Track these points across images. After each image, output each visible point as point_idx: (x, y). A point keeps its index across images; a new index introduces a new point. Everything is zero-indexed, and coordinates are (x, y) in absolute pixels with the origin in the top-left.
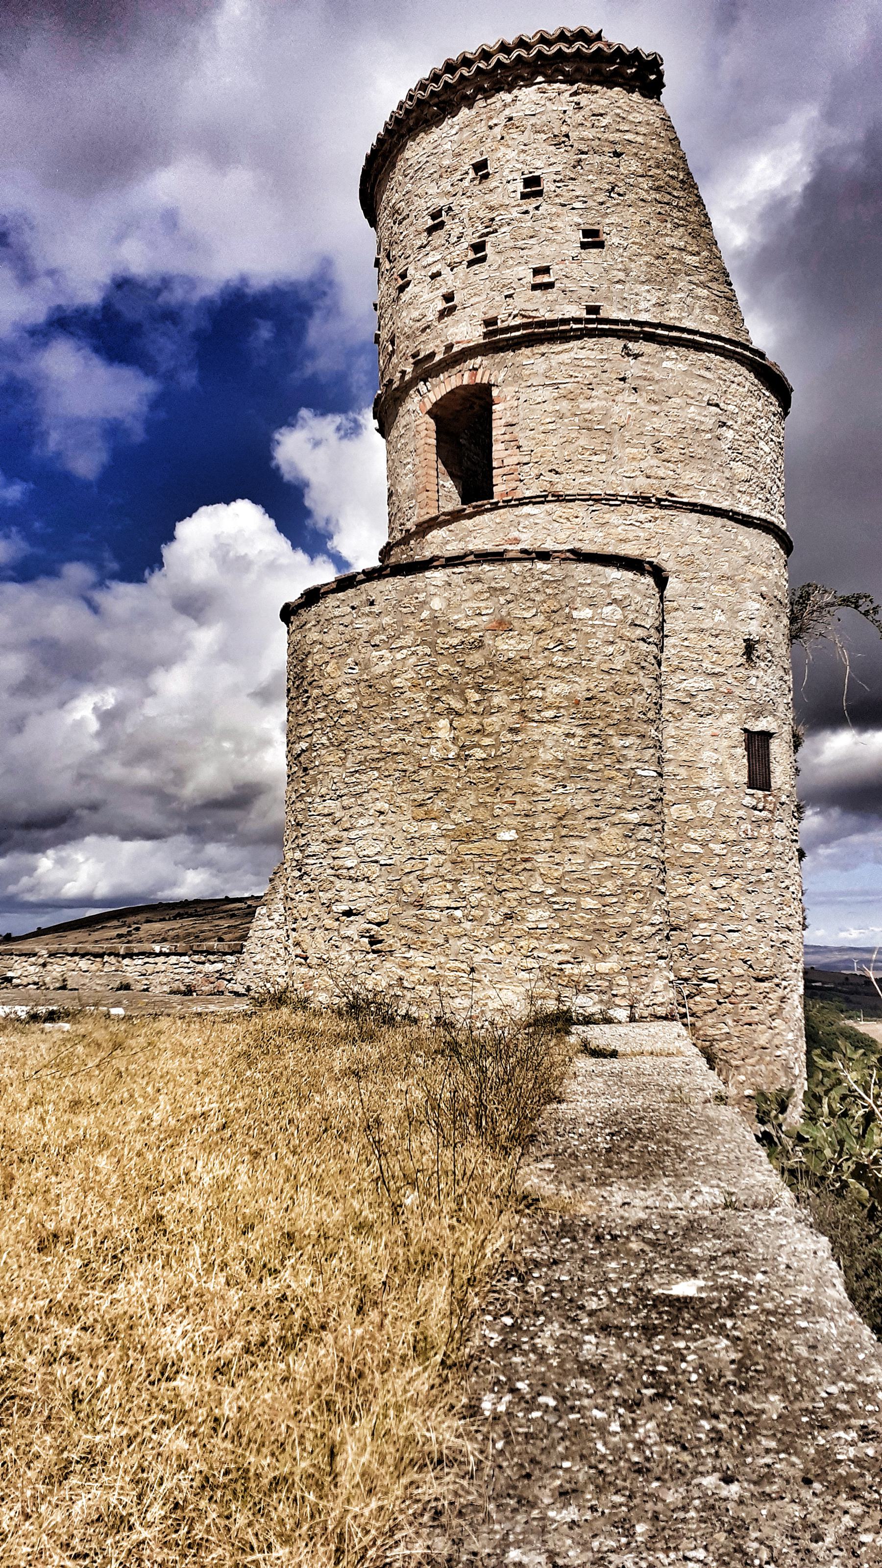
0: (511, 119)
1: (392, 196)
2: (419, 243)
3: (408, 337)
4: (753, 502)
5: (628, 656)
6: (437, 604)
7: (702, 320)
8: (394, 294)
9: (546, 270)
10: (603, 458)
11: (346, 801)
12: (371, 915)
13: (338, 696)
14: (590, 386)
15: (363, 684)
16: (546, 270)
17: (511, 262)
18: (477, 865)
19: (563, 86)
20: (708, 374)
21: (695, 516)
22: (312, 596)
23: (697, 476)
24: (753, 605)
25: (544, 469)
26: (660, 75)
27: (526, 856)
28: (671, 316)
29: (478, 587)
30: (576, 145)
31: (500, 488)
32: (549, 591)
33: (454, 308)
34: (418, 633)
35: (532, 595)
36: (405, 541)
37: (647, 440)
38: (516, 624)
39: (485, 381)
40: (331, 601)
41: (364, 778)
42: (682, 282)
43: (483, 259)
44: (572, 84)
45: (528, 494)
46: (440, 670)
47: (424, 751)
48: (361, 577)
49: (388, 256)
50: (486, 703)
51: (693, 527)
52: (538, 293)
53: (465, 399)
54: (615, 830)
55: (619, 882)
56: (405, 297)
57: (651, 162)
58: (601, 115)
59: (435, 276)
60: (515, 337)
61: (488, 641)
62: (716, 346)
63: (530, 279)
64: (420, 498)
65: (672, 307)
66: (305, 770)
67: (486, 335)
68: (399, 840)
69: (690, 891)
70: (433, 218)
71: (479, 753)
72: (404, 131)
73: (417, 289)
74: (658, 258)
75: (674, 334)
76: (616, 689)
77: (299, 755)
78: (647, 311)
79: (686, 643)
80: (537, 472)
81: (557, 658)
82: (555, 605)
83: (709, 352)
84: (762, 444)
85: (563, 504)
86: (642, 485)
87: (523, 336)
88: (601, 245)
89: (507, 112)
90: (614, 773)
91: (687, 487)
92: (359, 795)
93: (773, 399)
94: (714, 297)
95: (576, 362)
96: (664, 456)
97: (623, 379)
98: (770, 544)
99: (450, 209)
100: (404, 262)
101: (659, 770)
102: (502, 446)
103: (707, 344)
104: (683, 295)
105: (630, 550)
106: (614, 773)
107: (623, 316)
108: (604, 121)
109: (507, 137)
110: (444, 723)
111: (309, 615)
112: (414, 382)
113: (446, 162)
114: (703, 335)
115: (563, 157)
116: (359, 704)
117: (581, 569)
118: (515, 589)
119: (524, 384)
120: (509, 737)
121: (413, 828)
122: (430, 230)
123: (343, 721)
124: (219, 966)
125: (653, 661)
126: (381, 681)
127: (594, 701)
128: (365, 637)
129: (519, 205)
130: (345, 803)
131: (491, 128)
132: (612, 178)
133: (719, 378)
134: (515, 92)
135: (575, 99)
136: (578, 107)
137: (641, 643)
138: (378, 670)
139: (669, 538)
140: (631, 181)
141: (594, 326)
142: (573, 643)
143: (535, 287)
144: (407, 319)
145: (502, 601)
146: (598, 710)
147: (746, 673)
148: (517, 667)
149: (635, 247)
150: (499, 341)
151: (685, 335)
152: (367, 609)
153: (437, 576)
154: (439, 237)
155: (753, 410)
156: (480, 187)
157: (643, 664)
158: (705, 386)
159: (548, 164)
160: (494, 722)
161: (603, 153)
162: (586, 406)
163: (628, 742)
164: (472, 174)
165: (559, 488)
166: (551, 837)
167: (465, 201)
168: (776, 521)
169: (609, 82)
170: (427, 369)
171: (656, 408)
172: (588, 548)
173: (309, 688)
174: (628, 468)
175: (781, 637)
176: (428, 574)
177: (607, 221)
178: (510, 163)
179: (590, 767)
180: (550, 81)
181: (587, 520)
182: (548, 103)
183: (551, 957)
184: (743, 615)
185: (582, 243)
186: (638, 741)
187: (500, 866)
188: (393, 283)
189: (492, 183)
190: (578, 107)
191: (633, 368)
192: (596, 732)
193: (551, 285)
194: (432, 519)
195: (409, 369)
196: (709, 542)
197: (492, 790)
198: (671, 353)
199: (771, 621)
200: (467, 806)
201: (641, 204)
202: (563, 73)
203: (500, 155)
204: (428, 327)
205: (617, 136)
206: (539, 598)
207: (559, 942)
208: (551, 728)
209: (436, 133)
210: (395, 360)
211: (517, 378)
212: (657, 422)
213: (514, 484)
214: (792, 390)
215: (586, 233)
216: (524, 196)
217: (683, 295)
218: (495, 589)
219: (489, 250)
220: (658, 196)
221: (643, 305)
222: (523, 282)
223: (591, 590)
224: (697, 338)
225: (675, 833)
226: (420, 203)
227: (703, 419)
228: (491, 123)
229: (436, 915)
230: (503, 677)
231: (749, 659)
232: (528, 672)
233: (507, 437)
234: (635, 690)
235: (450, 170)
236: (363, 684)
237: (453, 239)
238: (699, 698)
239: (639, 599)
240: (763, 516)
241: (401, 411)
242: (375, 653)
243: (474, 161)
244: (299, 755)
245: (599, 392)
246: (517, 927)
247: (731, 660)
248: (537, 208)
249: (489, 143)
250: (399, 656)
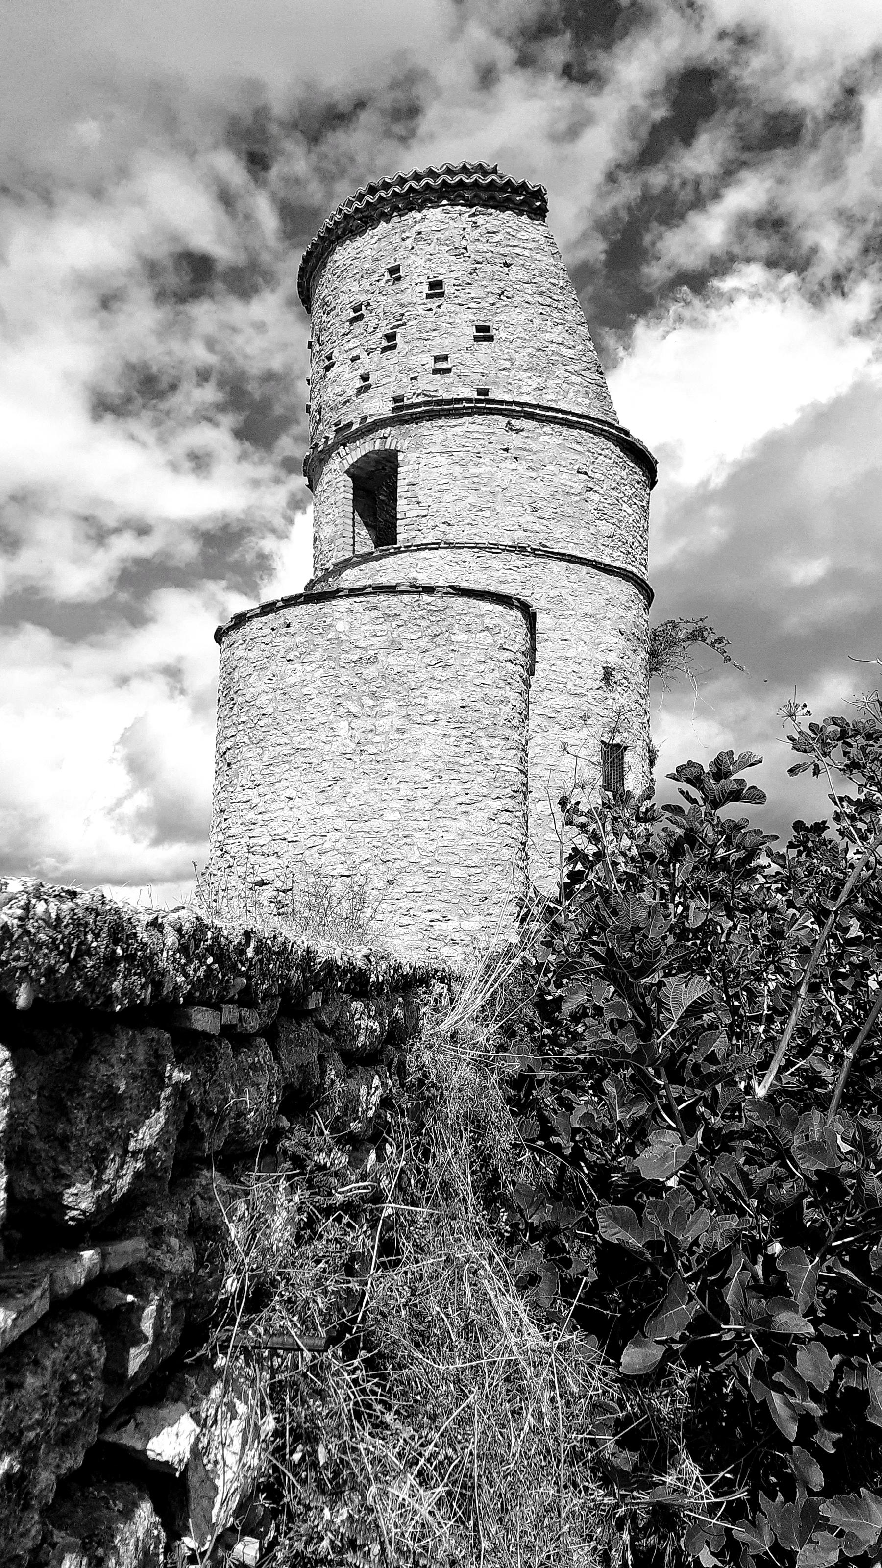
0: (420, 233)
1: (322, 291)
2: (343, 331)
4: (615, 555)
5: (496, 674)
6: (341, 626)
7: (574, 403)
8: (322, 372)
9: (445, 358)
10: (487, 513)
13: (258, 702)
14: (478, 455)
15: (279, 692)
16: (445, 358)
17: (416, 350)
18: (367, 841)
19: (464, 209)
20: (578, 448)
21: (564, 564)
22: (241, 620)
23: (567, 531)
24: (612, 639)
25: (439, 521)
26: (544, 201)
27: (407, 833)
28: (547, 399)
29: (375, 613)
30: (473, 256)
31: (402, 537)
32: (432, 619)
33: (370, 386)
34: (325, 650)
35: (419, 622)
36: (324, 578)
37: (526, 501)
38: (405, 644)
39: (393, 448)
40: (256, 623)
41: (276, 770)
42: (560, 371)
43: (394, 347)
44: (471, 207)
45: (425, 541)
46: (342, 680)
47: (327, 747)
48: (281, 604)
49: (318, 340)
50: (378, 708)
51: (562, 573)
52: (438, 376)
53: (377, 462)
54: (481, 814)
55: (483, 857)
56: (330, 375)
57: (536, 272)
58: (494, 233)
59: (354, 359)
60: (416, 413)
61: (381, 657)
62: (586, 425)
64: (337, 543)
65: (550, 391)
66: (229, 765)
67: (394, 410)
68: (304, 822)
69: (550, 873)
70: (355, 311)
72: (333, 238)
73: (340, 369)
74: (539, 350)
75: (550, 413)
76: (486, 700)
77: (225, 753)
78: (528, 394)
79: (553, 668)
80: (433, 524)
82: (436, 630)
83: (580, 429)
84: (625, 507)
85: (454, 551)
86: (519, 537)
87: (426, 411)
88: (491, 338)
89: (417, 227)
90: (481, 768)
91: (557, 541)
93: (638, 470)
94: (586, 384)
95: (468, 435)
96: (539, 514)
97: (507, 450)
98: (628, 589)
99: (368, 304)
100: (330, 346)
101: (521, 768)
102: (404, 502)
103: (578, 422)
104: (560, 381)
105: (507, 590)
106: (481, 768)
107: (507, 398)
108: (497, 238)
109: (416, 248)
110: (344, 724)
111: (236, 636)
112: (335, 446)
113: (367, 266)
114: (574, 414)
115: (463, 266)
117: (460, 602)
118: (404, 616)
119: (425, 451)
120: (397, 736)
122: (352, 321)
123: (261, 723)
125: (519, 679)
126: (293, 689)
127: (467, 709)
128: (282, 653)
129: (424, 304)
130: (260, 791)
131: (403, 239)
132: (502, 284)
133: (589, 451)
134: (424, 212)
135: (473, 219)
136: (475, 225)
137: (509, 664)
138: (292, 680)
139: (543, 583)
140: (518, 287)
141: (483, 405)
142: (451, 661)
143: (436, 372)
144: (331, 394)
146: (470, 716)
147: (605, 695)
148: (404, 679)
149: (520, 341)
150: (405, 414)
151: (560, 415)
153: (343, 604)
154: (359, 327)
155: (618, 478)
156: (394, 287)
157: (510, 680)
158: (576, 457)
159: (450, 270)
160: (384, 724)
161: (495, 264)
162: (474, 470)
163: (495, 742)
164: (387, 276)
165: (450, 538)
166: (427, 818)
167: (381, 298)
168: (635, 571)
169: (501, 206)
170: (346, 435)
171: (534, 474)
172: (465, 585)
173: (235, 696)
174: (510, 522)
175: (638, 668)
176: (334, 602)
177: (497, 319)
178: (418, 268)
179: (462, 762)
180: (453, 204)
181: (473, 564)
182: (451, 222)
183: (424, 916)
184: (603, 647)
185: (475, 337)
186: (503, 743)
188: (321, 363)
189: (403, 284)
190: (475, 225)
191: (515, 441)
192: (468, 734)
193: (448, 370)
194: (346, 560)
195: (332, 436)
196: (575, 585)
197: (381, 780)
198: (547, 429)
199: (628, 653)
200: (360, 792)
201: (527, 305)
202: (464, 198)
203: (410, 262)
204: (348, 401)
205: (507, 250)
206: (424, 623)
208: (432, 730)
209: (359, 241)
210: (321, 427)
211: (418, 446)
212: (534, 485)
213: (414, 533)
214: (657, 462)
215: (479, 329)
216: (429, 296)
217: (560, 381)
218: (389, 616)
219: (399, 339)
220: (541, 300)
222: (426, 367)
223: (467, 619)
224: (570, 417)
225: (539, 825)
226: (345, 299)
227: (573, 484)
228: (404, 236)
230: (392, 686)
231: (607, 684)
232: (413, 683)
233: (409, 494)
234: (502, 702)
235: (369, 273)
236: (279, 692)
237: (370, 330)
238: (563, 714)
239: (507, 628)
240: (623, 566)
241: (325, 470)
242: (289, 667)
243: (389, 266)
244: (225, 753)
245: (486, 459)
246: (397, 891)
247: (591, 684)
248: (439, 306)
249: (401, 252)
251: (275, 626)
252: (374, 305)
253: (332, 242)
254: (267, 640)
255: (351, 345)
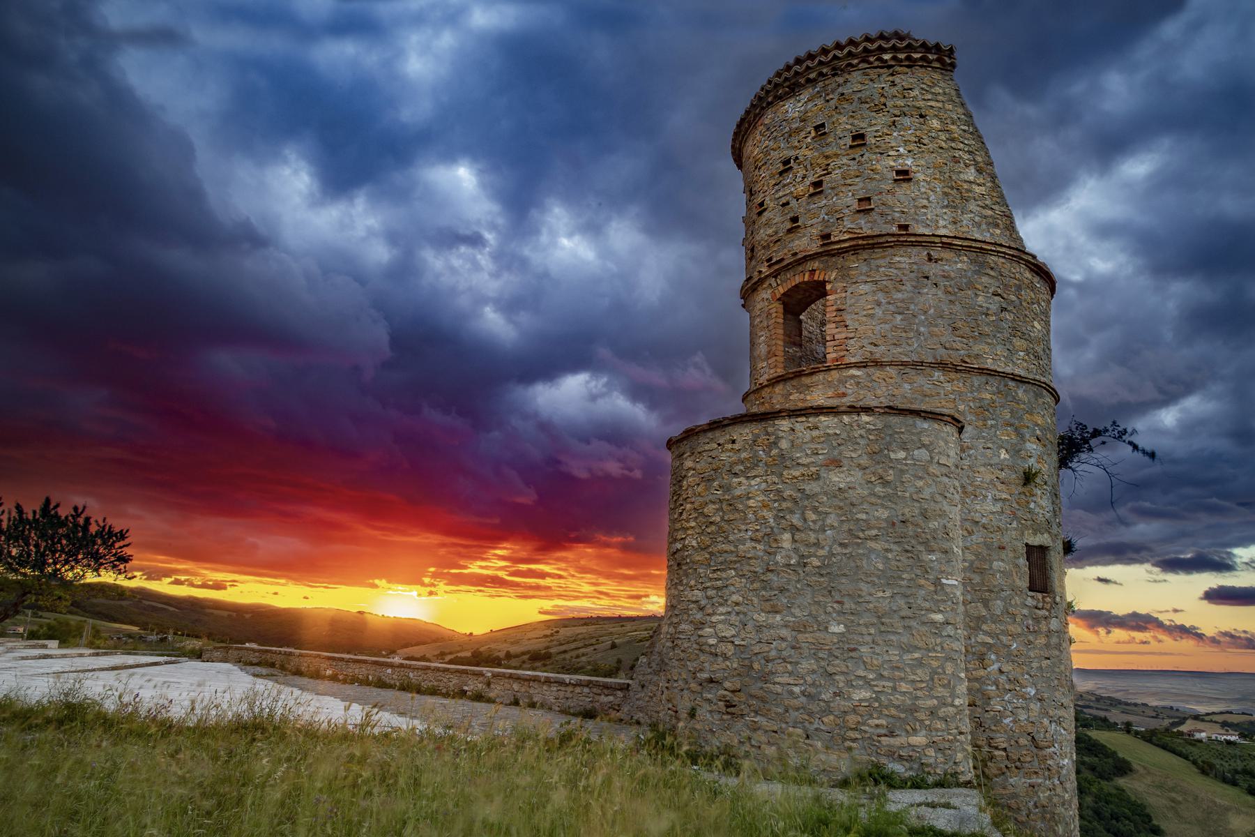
1: (752, 149)
3: (764, 248)
6: (784, 444)
11: (711, 593)
12: (727, 684)
16: (869, 199)
20: (992, 273)
25: (865, 342)
38: (845, 462)
41: (724, 575)
45: (853, 360)
61: (823, 474)
63: (855, 206)
71: (816, 562)
78: (945, 227)
81: (878, 489)
89: (840, 90)
92: (718, 589)
99: (797, 158)
111: (685, 447)
113: (794, 126)
116: (722, 519)
117: (895, 420)
118: (844, 435)
120: (839, 549)
121: (762, 617)
123: (709, 530)
124: (611, 698)
138: (737, 492)
145: (835, 444)
152: (730, 446)
153: (784, 424)
171: (952, 298)
185: (896, 180)
187: (831, 654)
190: (893, 84)
191: (932, 269)
207: (878, 718)
215: (898, 172)
221: (941, 223)
229: (778, 689)
250: (753, 483)
251: (721, 441)
252: (801, 159)
253: (763, 108)
254: (713, 454)
255: (781, 194)
